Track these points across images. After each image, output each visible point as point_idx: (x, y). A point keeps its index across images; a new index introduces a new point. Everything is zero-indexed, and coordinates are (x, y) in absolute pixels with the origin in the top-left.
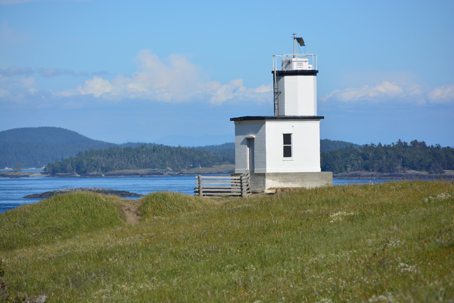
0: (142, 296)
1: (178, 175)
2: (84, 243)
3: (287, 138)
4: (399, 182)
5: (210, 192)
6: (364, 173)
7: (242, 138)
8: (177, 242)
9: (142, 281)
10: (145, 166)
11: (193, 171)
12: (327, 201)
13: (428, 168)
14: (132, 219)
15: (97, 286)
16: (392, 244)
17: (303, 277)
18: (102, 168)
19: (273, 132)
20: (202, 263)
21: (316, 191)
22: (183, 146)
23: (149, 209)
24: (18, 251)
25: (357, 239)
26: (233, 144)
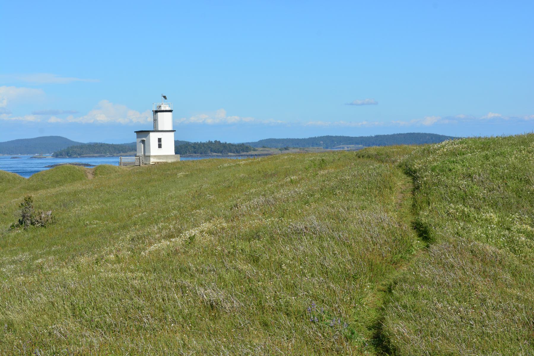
0: (94, 211)
1: (112, 157)
2: (68, 188)
3: (160, 140)
4: (208, 159)
5: (125, 164)
6: (195, 155)
7: (140, 139)
8: (109, 187)
9: (94, 204)
10: (97, 153)
11: (119, 155)
12: (177, 168)
13: (221, 152)
14: (90, 177)
15: (74, 206)
16: (204, 186)
17: (166, 202)
18: (78, 154)
19: (153, 137)
20: (120, 196)
21: (172, 163)
22: (114, 144)
23: (98, 172)
24: (39, 191)
25: (189, 185)
26: (136, 143)
